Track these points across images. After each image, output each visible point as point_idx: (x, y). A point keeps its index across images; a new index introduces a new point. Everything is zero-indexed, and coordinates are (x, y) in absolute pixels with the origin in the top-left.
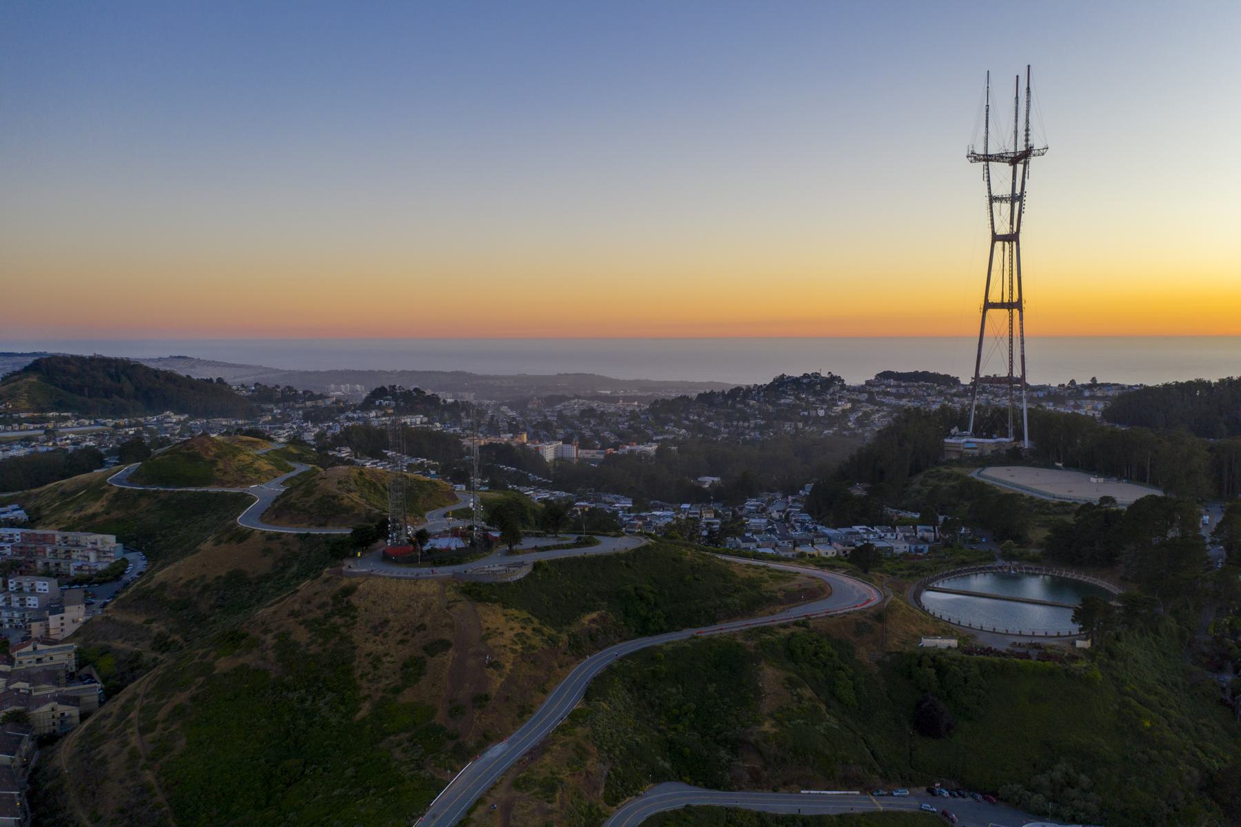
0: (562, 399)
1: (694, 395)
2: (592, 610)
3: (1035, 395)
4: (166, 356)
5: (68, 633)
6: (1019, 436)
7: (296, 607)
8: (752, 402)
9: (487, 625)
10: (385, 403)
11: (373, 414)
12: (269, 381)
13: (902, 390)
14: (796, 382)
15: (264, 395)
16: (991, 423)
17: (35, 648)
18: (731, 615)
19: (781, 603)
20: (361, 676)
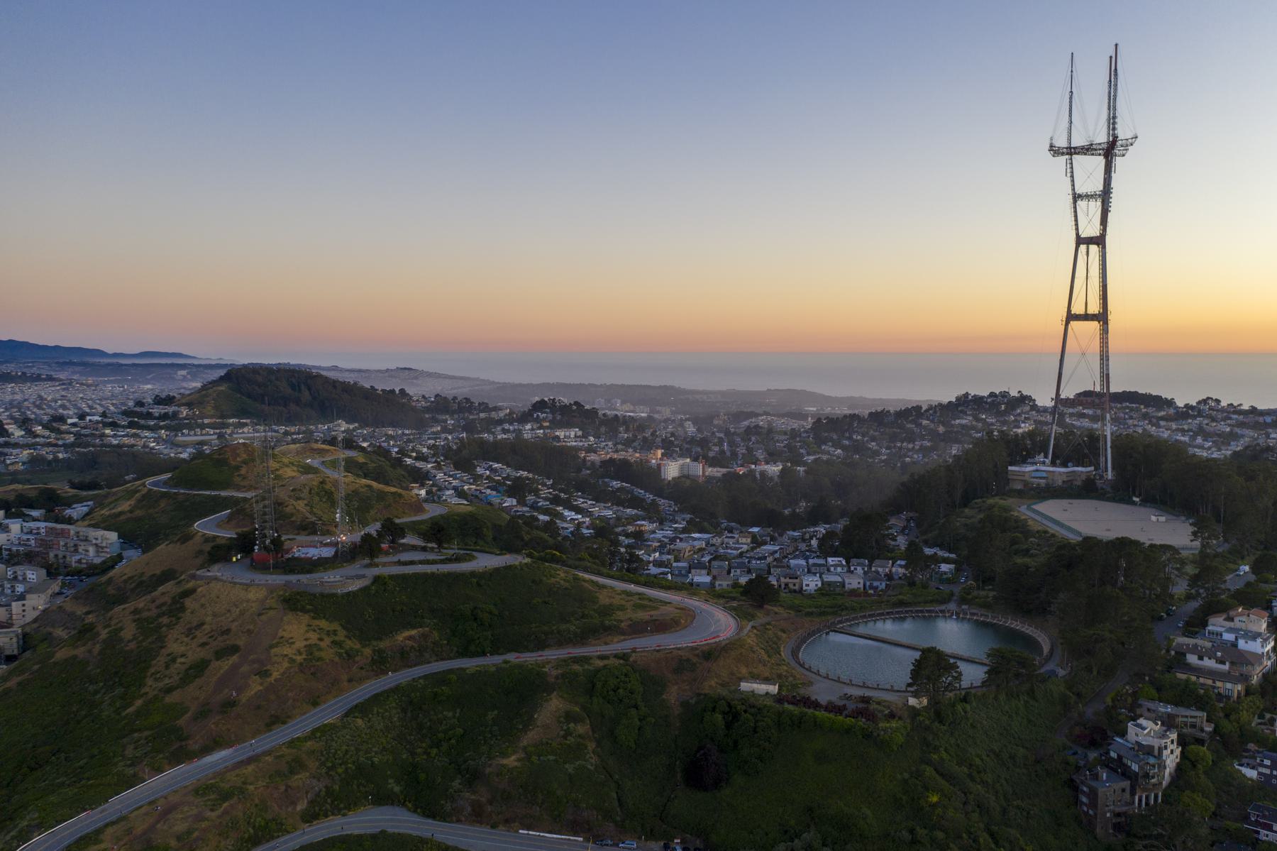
1: (866, 413)
2: (414, 627)
3: (1261, 419)
4: (393, 367)
9: (285, 634)
10: (542, 416)
11: (528, 427)
12: (447, 390)
14: (978, 400)
15: (441, 405)
16: (1079, 449)
19: (623, 633)
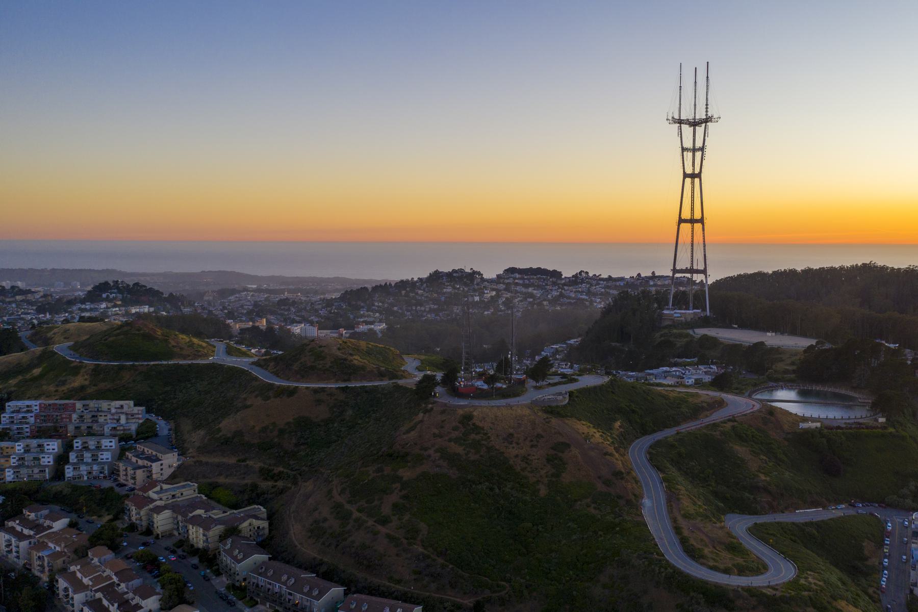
0: (233, 292)
3: (618, 284)
5: (165, 477)
6: (704, 309)
8: (420, 292)
17: (161, 488)
18: (687, 418)
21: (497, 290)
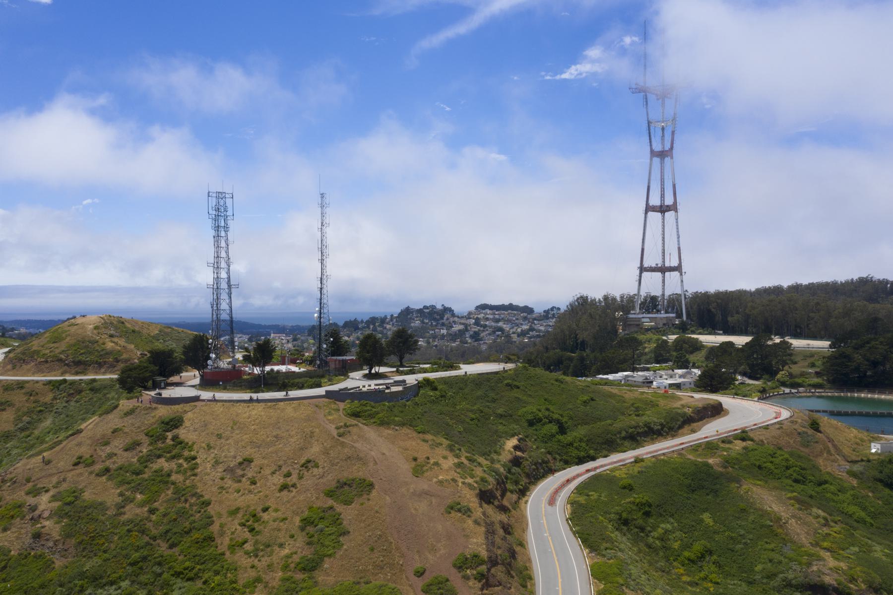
1: (341, 324)
7: (85, 451)
13: (497, 316)
18: (653, 433)
20: (232, 547)
21: (466, 325)
